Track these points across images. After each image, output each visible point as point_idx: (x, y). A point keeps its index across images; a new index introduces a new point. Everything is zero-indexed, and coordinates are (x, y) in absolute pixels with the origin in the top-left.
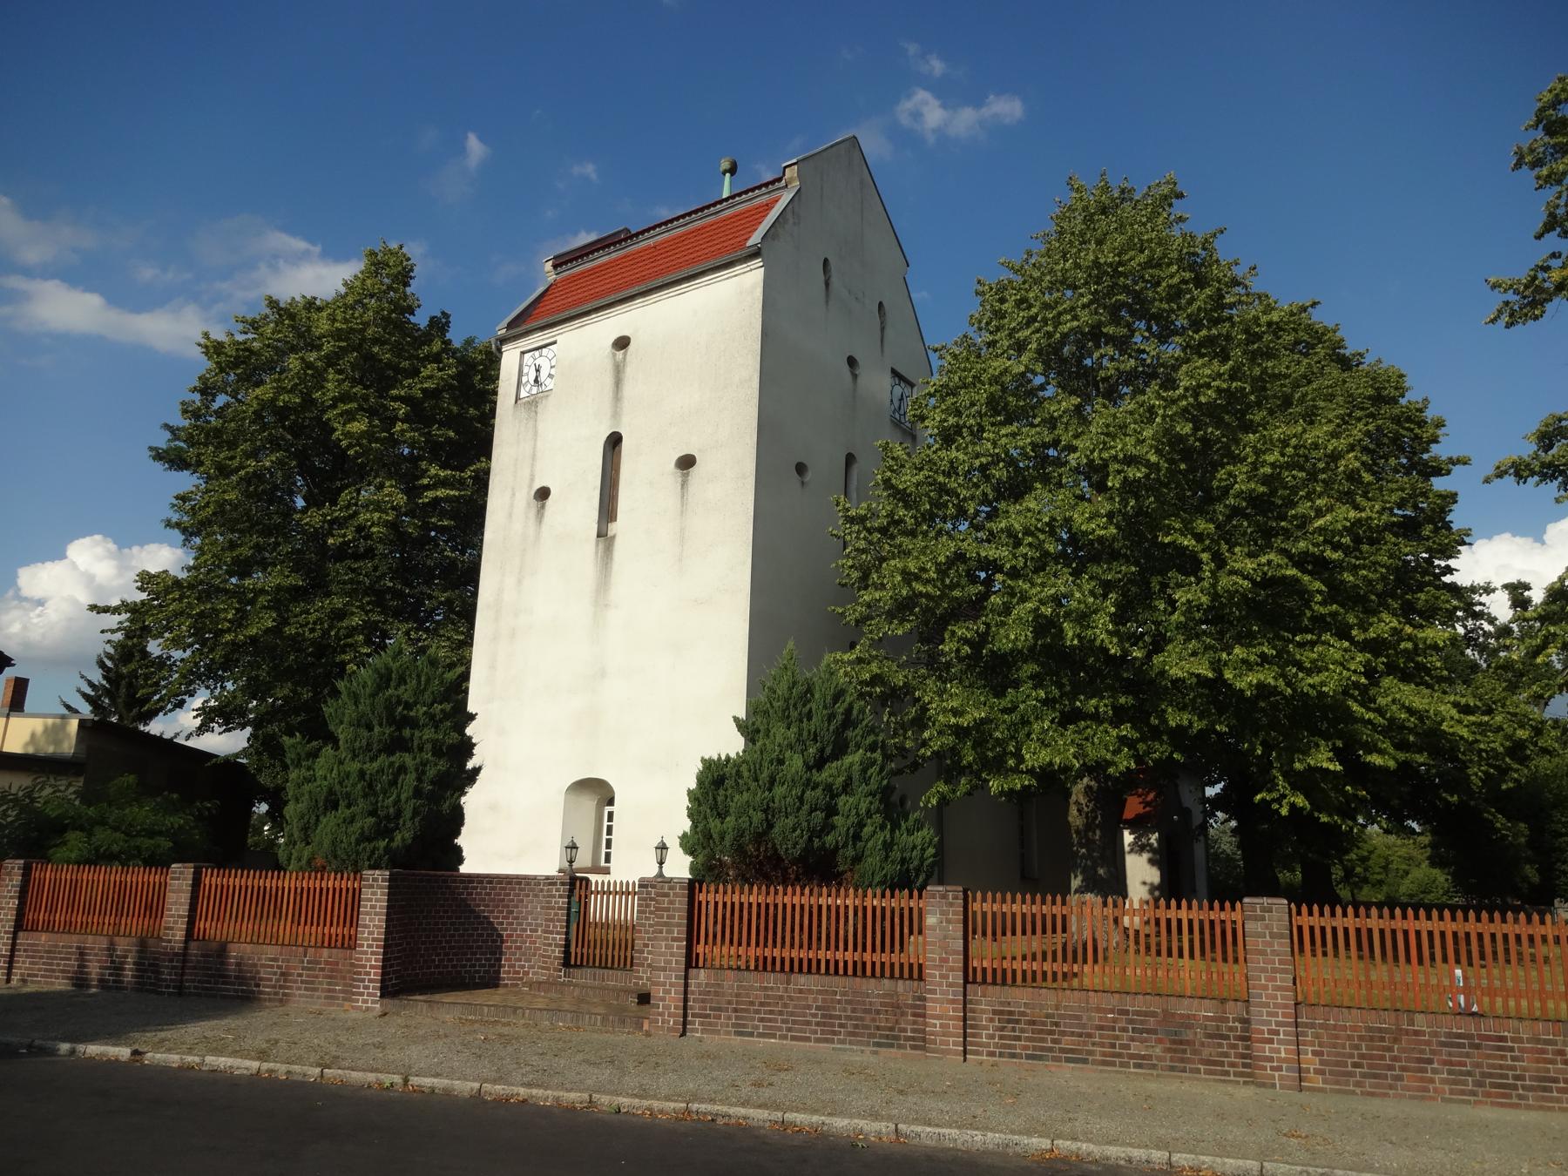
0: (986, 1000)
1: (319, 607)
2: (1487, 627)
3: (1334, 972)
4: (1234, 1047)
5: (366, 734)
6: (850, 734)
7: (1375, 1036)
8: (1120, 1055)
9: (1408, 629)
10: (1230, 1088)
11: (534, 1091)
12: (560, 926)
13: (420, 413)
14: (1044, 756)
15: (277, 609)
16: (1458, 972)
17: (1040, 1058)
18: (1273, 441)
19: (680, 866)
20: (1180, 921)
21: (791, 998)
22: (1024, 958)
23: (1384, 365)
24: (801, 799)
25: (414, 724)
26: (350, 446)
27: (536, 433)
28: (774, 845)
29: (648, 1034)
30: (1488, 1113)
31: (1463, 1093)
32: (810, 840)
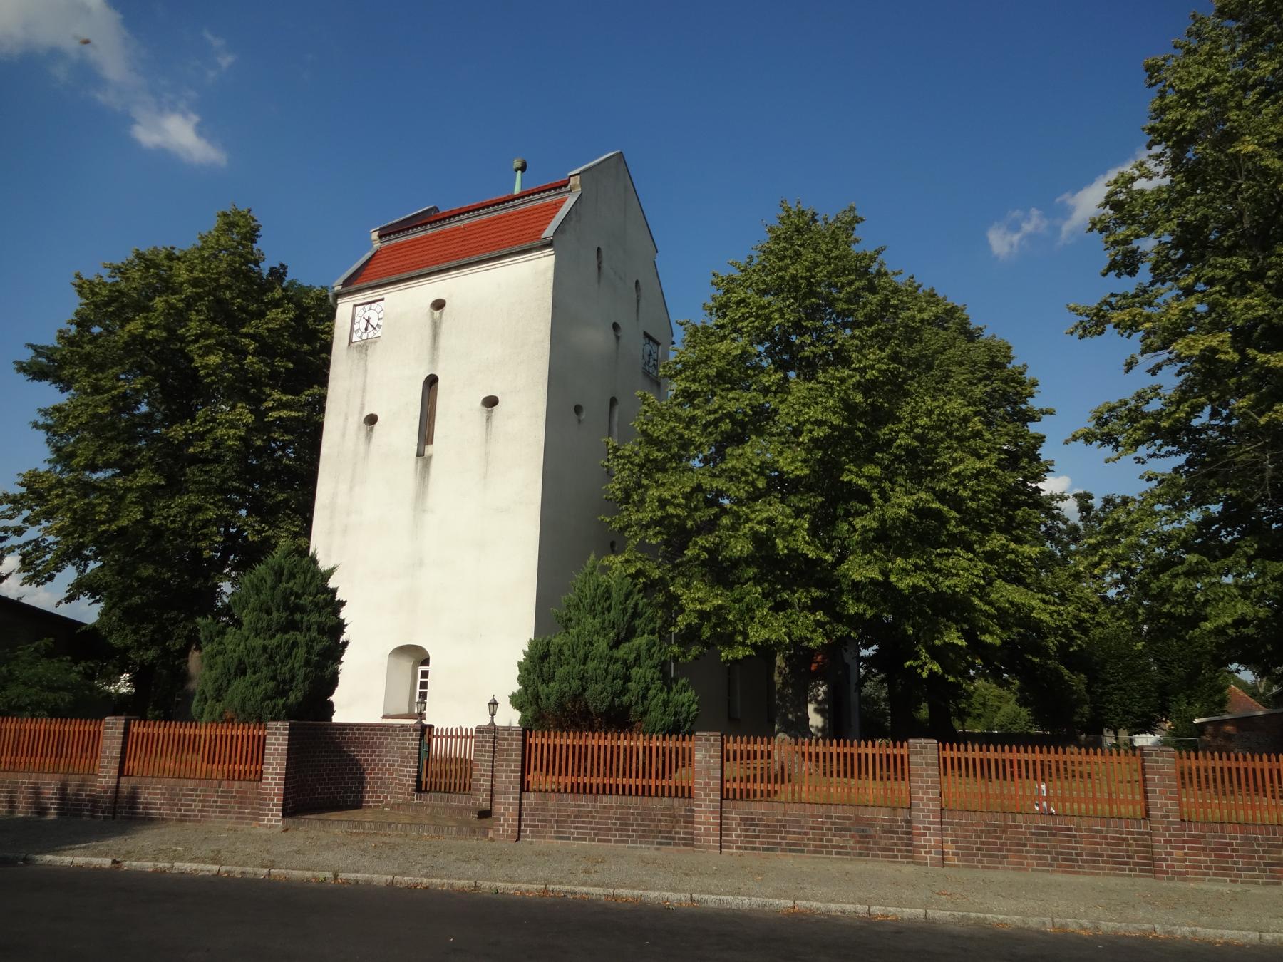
0: (736, 811)
1: (181, 502)
2: (1062, 526)
3: (966, 788)
4: (902, 839)
5: (266, 617)
6: (637, 622)
7: (990, 829)
8: (826, 847)
9: (1013, 545)
10: (898, 866)
11: (434, 881)
12: (413, 762)
13: (266, 349)
14: (764, 634)
15: (142, 504)
16: (1043, 787)
17: (772, 850)
18: (922, 408)
19: (509, 717)
20: (867, 755)
21: (597, 812)
22: (741, 780)
23: (997, 339)
24: (606, 670)
25: (302, 609)
26: (208, 375)
27: (366, 365)
28: (586, 704)
29: (492, 840)
30: (1059, 878)
31: (1045, 865)
32: (613, 700)
